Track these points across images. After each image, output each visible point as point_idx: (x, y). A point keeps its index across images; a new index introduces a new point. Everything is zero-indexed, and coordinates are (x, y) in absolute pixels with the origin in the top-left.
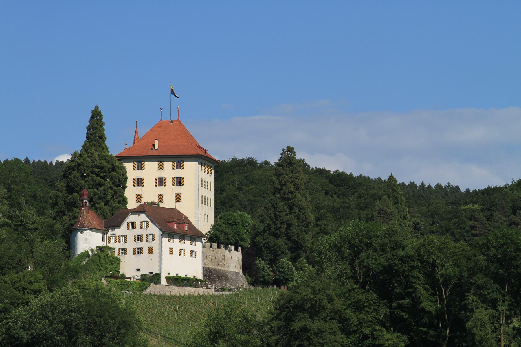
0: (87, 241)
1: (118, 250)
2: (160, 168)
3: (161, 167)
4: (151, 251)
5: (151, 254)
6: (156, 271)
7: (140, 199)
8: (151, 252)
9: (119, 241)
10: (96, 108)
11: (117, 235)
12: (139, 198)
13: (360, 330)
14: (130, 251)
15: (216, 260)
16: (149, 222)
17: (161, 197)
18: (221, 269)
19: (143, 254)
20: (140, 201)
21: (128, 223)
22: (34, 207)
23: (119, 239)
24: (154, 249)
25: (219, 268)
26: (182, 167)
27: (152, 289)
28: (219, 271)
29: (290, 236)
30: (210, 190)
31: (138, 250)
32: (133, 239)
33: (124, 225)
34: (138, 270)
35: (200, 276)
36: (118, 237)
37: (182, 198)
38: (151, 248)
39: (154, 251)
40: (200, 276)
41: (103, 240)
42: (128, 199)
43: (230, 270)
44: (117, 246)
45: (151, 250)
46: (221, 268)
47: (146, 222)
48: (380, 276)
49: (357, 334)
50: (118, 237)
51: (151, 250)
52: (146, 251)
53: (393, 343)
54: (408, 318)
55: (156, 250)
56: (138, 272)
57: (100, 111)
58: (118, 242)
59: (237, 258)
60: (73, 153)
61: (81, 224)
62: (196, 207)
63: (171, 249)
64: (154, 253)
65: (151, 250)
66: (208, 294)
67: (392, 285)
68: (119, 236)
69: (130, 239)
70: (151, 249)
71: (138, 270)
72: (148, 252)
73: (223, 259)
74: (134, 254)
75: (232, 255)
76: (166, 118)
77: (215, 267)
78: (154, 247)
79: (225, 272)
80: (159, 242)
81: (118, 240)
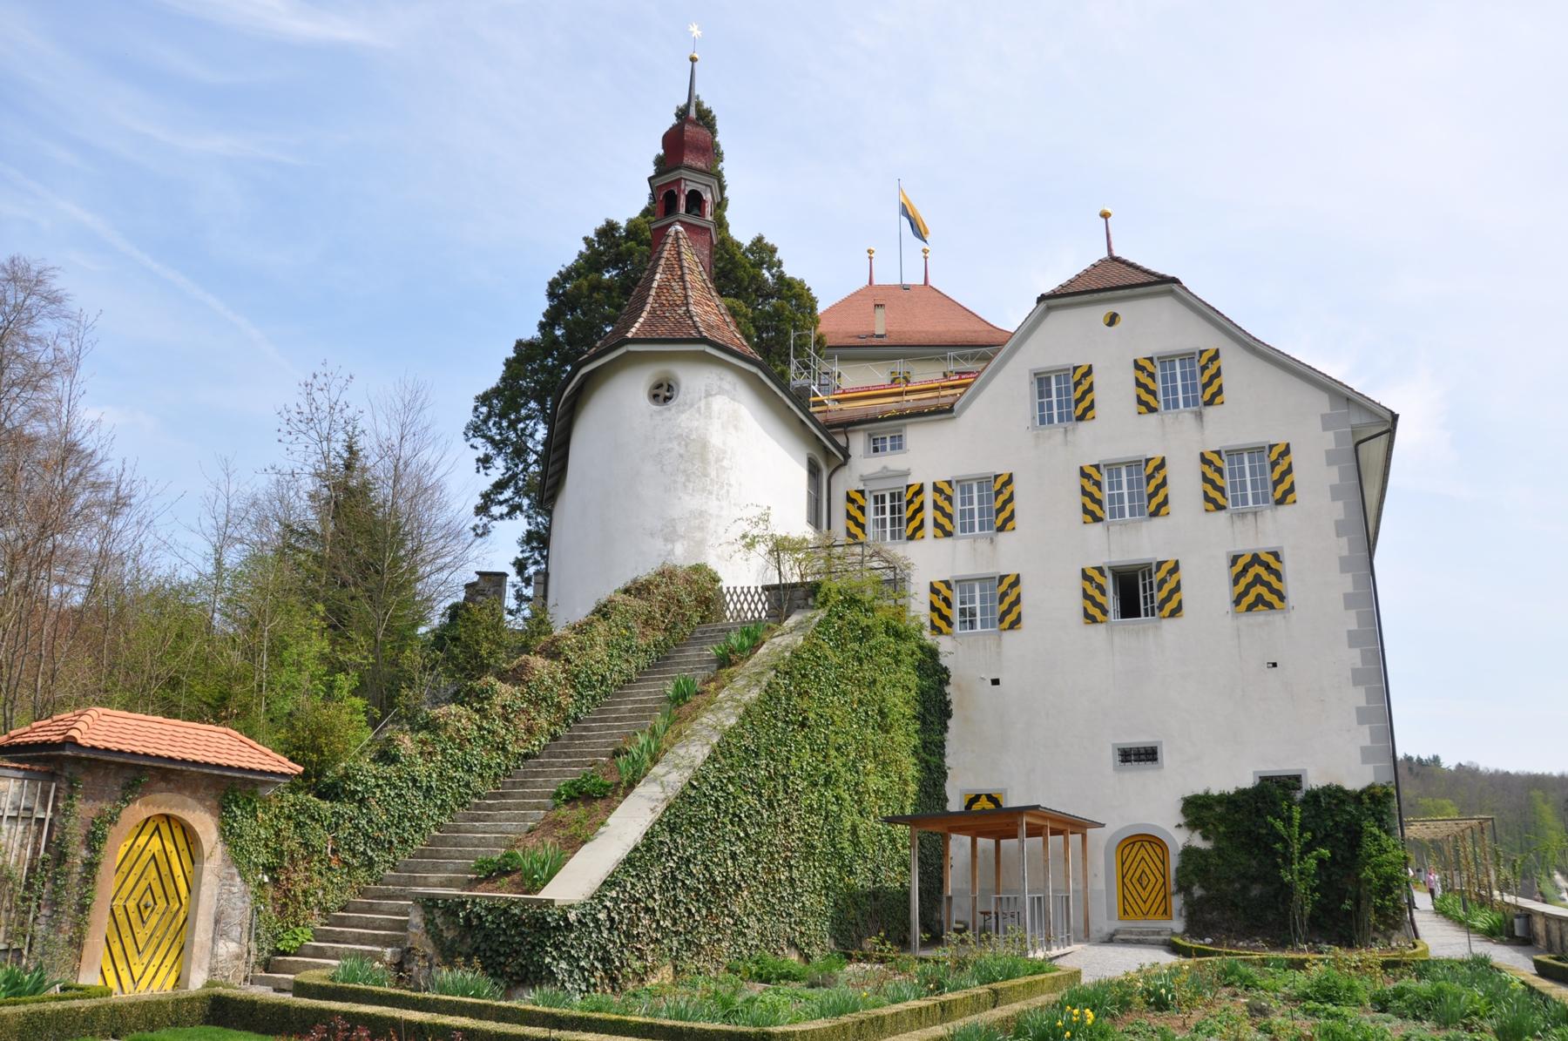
5: (1261, 617)
7: (1268, 585)
8: (1260, 599)
9: (937, 525)
12: (1258, 579)
13: (599, 980)
16: (1216, 356)
20: (1268, 596)
22: (672, 763)
23: (936, 506)
24: (1289, 568)
27: (976, 807)
29: (92, 590)
36: (929, 490)
38: (1255, 559)
39: (1291, 586)
45: (1258, 579)
47: (1187, 357)
49: (525, 443)
50: (929, 496)
56: (1140, 775)
66: (344, 441)
68: (936, 489)
78: (1287, 556)
81: (929, 514)
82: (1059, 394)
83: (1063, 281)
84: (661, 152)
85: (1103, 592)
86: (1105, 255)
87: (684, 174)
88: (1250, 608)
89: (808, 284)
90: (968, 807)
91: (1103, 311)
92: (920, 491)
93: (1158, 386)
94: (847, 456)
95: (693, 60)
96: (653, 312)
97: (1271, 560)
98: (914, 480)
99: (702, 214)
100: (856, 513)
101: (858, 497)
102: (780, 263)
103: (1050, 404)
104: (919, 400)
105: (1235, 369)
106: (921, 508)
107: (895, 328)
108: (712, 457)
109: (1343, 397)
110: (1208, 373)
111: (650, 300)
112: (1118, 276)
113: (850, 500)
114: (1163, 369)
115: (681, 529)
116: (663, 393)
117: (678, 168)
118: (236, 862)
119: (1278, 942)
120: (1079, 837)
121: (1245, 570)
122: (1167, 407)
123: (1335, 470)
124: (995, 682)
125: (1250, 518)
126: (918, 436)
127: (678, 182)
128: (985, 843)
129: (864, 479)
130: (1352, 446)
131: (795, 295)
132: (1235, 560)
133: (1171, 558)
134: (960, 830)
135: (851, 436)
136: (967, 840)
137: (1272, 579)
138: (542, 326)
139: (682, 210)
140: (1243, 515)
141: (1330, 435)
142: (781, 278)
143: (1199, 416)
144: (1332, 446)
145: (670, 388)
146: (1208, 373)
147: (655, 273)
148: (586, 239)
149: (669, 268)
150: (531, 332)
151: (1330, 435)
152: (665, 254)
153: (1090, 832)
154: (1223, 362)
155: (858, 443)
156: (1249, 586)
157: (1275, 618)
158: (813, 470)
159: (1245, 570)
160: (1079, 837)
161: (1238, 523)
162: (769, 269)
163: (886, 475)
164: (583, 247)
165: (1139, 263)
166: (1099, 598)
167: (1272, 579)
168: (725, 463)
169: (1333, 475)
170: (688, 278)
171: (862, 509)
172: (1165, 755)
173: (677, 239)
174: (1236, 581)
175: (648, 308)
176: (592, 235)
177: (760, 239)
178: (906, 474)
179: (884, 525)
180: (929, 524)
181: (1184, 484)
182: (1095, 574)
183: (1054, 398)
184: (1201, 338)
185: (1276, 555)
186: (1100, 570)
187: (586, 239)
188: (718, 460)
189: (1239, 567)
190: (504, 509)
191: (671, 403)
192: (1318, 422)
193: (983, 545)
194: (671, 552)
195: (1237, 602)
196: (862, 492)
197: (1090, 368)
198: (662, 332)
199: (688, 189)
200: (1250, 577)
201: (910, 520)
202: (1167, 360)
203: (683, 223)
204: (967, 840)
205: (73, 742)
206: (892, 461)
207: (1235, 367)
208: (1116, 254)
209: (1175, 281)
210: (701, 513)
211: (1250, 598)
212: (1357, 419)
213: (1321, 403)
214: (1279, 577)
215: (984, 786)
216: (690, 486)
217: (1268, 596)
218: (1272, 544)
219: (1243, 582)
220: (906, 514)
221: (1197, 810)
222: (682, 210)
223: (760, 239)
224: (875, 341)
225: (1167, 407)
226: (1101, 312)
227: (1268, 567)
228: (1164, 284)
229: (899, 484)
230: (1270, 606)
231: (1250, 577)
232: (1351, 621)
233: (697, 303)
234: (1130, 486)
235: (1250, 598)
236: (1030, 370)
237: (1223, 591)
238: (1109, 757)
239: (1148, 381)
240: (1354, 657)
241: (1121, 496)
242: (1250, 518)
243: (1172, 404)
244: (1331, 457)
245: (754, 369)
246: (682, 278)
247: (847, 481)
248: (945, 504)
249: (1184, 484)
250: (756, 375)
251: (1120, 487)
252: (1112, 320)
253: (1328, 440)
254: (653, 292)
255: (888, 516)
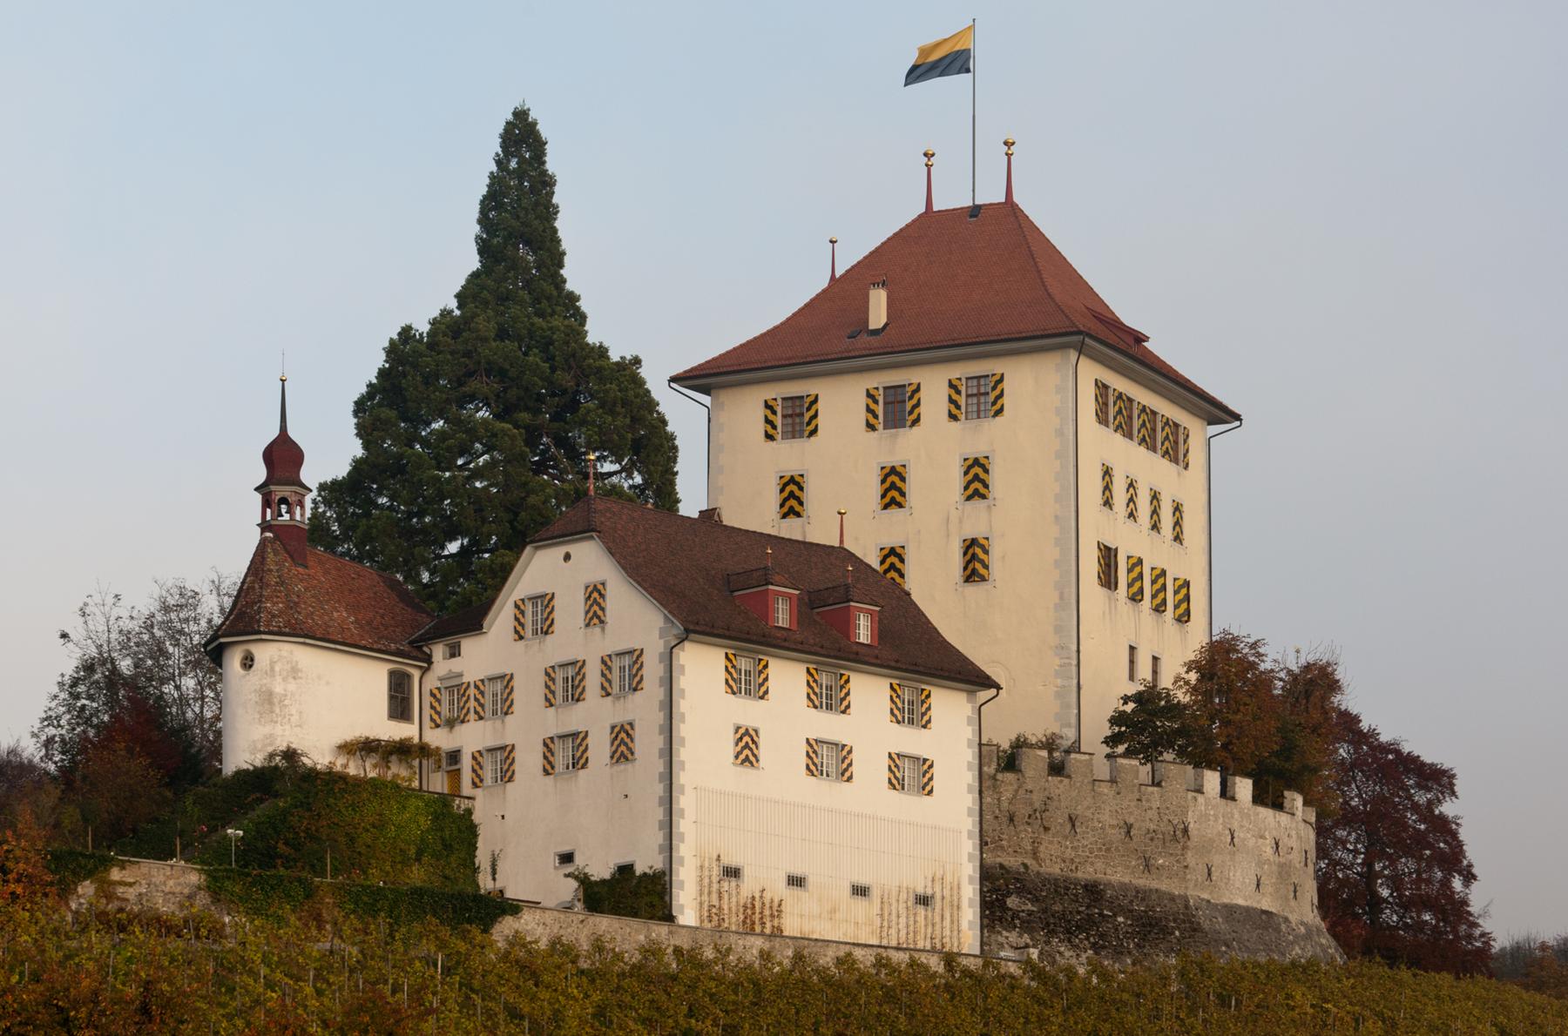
0: (271, 703)
1: (474, 758)
2: (970, 491)
3: (977, 485)
6: (646, 862)
10: (521, 115)
11: (469, 677)
14: (528, 760)
15: (1133, 845)
17: (792, 495)
18: (1163, 887)
21: (517, 606)
25: (1142, 882)
26: (994, 403)
28: (1142, 894)
30: (1107, 472)
32: (542, 690)
33: (501, 619)
37: (995, 559)
41: (400, 707)
43: (1226, 901)
44: (471, 737)
46: (1164, 885)
50: (472, 691)
52: (599, 747)
53: (941, 969)
55: (647, 743)
58: (472, 716)
59: (1269, 842)
62: (1061, 597)
63: (747, 733)
64: (636, 756)
69: (528, 692)
73: (1175, 839)
74: (546, 773)
75: (1235, 826)
76: (950, 198)
77: (1126, 880)
78: (761, 733)
79: (1187, 907)
80: (660, 694)
81: (472, 703)
84: (562, 272)
95: (283, 381)
98: (465, 680)
104: (1154, 381)
116: (248, 662)
119: (1008, 980)
129: (441, 679)
132: (613, 728)
137: (753, 746)
167: (753, 746)
177: (637, 361)
178: (460, 675)
191: (253, 669)
196: (439, 689)
199: (277, 498)
211: (742, 757)
214: (632, 741)
216: (263, 720)
218: (629, 718)
223: (637, 361)
227: (628, 734)
235: (742, 757)
236: (879, 463)
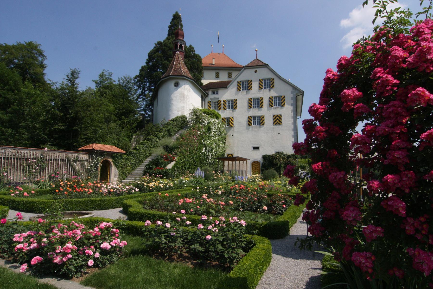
4: (278, 121)
7: (279, 120)
8: (277, 122)
12: (277, 119)
16: (273, 79)
19: (263, 124)
20: (279, 122)
27: (229, 156)
31: (257, 100)
34: (256, 148)
35: (375, 16)
36: (222, 102)
38: (277, 116)
39: (283, 121)
40: (375, 16)
42: (178, 115)
45: (277, 119)
47: (269, 79)
48: (386, 66)
50: (222, 102)
51: (277, 120)
52: (269, 121)
54: (423, 277)
56: (256, 151)
57: (191, 46)
60: (97, 78)
61: (175, 71)
65: (277, 120)
67: (394, 94)
68: (224, 101)
70: (278, 117)
71: (256, 148)
72: (272, 123)
78: (283, 115)
81: (222, 106)
82: (246, 85)
83: (248, 64)
85: (251, 121)
86: (255, 58)
87: (179, 41)
88: (276, 124)
89: (200, 55)
90: (227, 156)
91: (254, 70)
92: (221, 101)
93: (263, 85)
94: (208, 95)
96: (174, 69)
97: (280, 116)
99: (182, 49)
100: (209, 105)
101: (210, 102)
102: (195, 51)
103: (244, 87)
105: (277, 82)
106: (221, 105)
107: (217, 63)
108: (185, 97)
109: (295, 88)
110: (272, 82)
111: (174, 67)
112: (258, 63)
113: (208, 103)
114: (264, 81)
115: (180, 109)
117: (178, 40)
118: (116, 167)
120: (245, 161)
121: (275, 118)
122: (264, 88)
123: (292, 101)
124: (233, 135)
125: (277, 109)
126: (220, 91)
127: (178, 42)
128: (230, 162)
129: (211, 99)
130: (295, 97)
131: (198, 59)
132: (274, 116)
133: (263, 115)
134: (226, 160)
135: (209, 91)
136: (227, 162)
137: (280, 119)
138: (146, 63)
139: (179, 48)
140: (276, 108)
141: (292, 94)
142: (195, 54)
143: (270, 90)
144: (292, 96)
145: (178, 84)
146: (272, 82)
147: (174, 61)
148: (155, 44)
149: (177, 61)
150: (144, 64)
151: (292, 94)
152: (176, 58)
153: (247, 160)
154: (275, 80)
155: (210, 93)
156: (276, 121)
157: (280, 126)
158: (202, 98)
159: (275, 118)
160: (245, 161)
161: (275, 109)
162: (192, 52)
163: (215, 98)
164: (155, 46)
165: (262, 61)
166: (250, 121)
167: (280, 119)
168: (188, 98)
169: (292, 102)
170: (180, 63)
171: (210, 104)
172: (260, 148)
173: (178, 55)
174: (274, 120)
175: (173, 68)
176: (156, 43)
178: (218, 98)
179: (214, 107)
180: (222, 108)
181: (266, 102)
182: (250, 118)
183: (245, 86)
184: (271, 76)
185: (281, 115)
186: (251, 117)
187: (155, 44)
188: (186, 97)
189: (274, 117)
190: (141, 99)
192: (290, 92)
193: (231, 111)
194: (178, 113)
195: (274, 123)
196: (210, 101)
197: (251, 80)
198: (176, 74)
200: (276, 119)
201: (219, 107)
202: (265, 80)
203: (179, 51)
204: (227, 162)
205: (94, 149)
206: (216, 96)
207: (277, 82)
208: (257, 58)
209: (268, 65)
210: (184, 107)
211: (276, 122)
212: (297, 92)
213: (291, 89)
214: (281, 119)
215: (230, 153)
217: (279, 122)
219: (275, 120)
220: (218, 106)
221: (264, 157)
222: (179, 48)
224: (212, 66)
225: (264, 88)
226: (254, 70)
228: (265, 66)
229: (217, 100)
230: (279, 124)
231: (276, 119)
232: (292, 127)
233: (182, 68)
234: (257, 102)
235: (276, 122)
237: (271, 121)
238: (251, 148)
239: (261, 83)
240: (292, 133)
241: (255, 104)
242: (277, 109)
243: (265, 88)
244: (292, 99)
245: (192, 81)
246: (179, 63)
247: (208, 99)
248: (225, 104)
249: (266, 102)
250: (193, 82)
251: (255, 102)
252: (256, 72)
253: (292, 95)
254: (174, 66)
255: (215, 106)
